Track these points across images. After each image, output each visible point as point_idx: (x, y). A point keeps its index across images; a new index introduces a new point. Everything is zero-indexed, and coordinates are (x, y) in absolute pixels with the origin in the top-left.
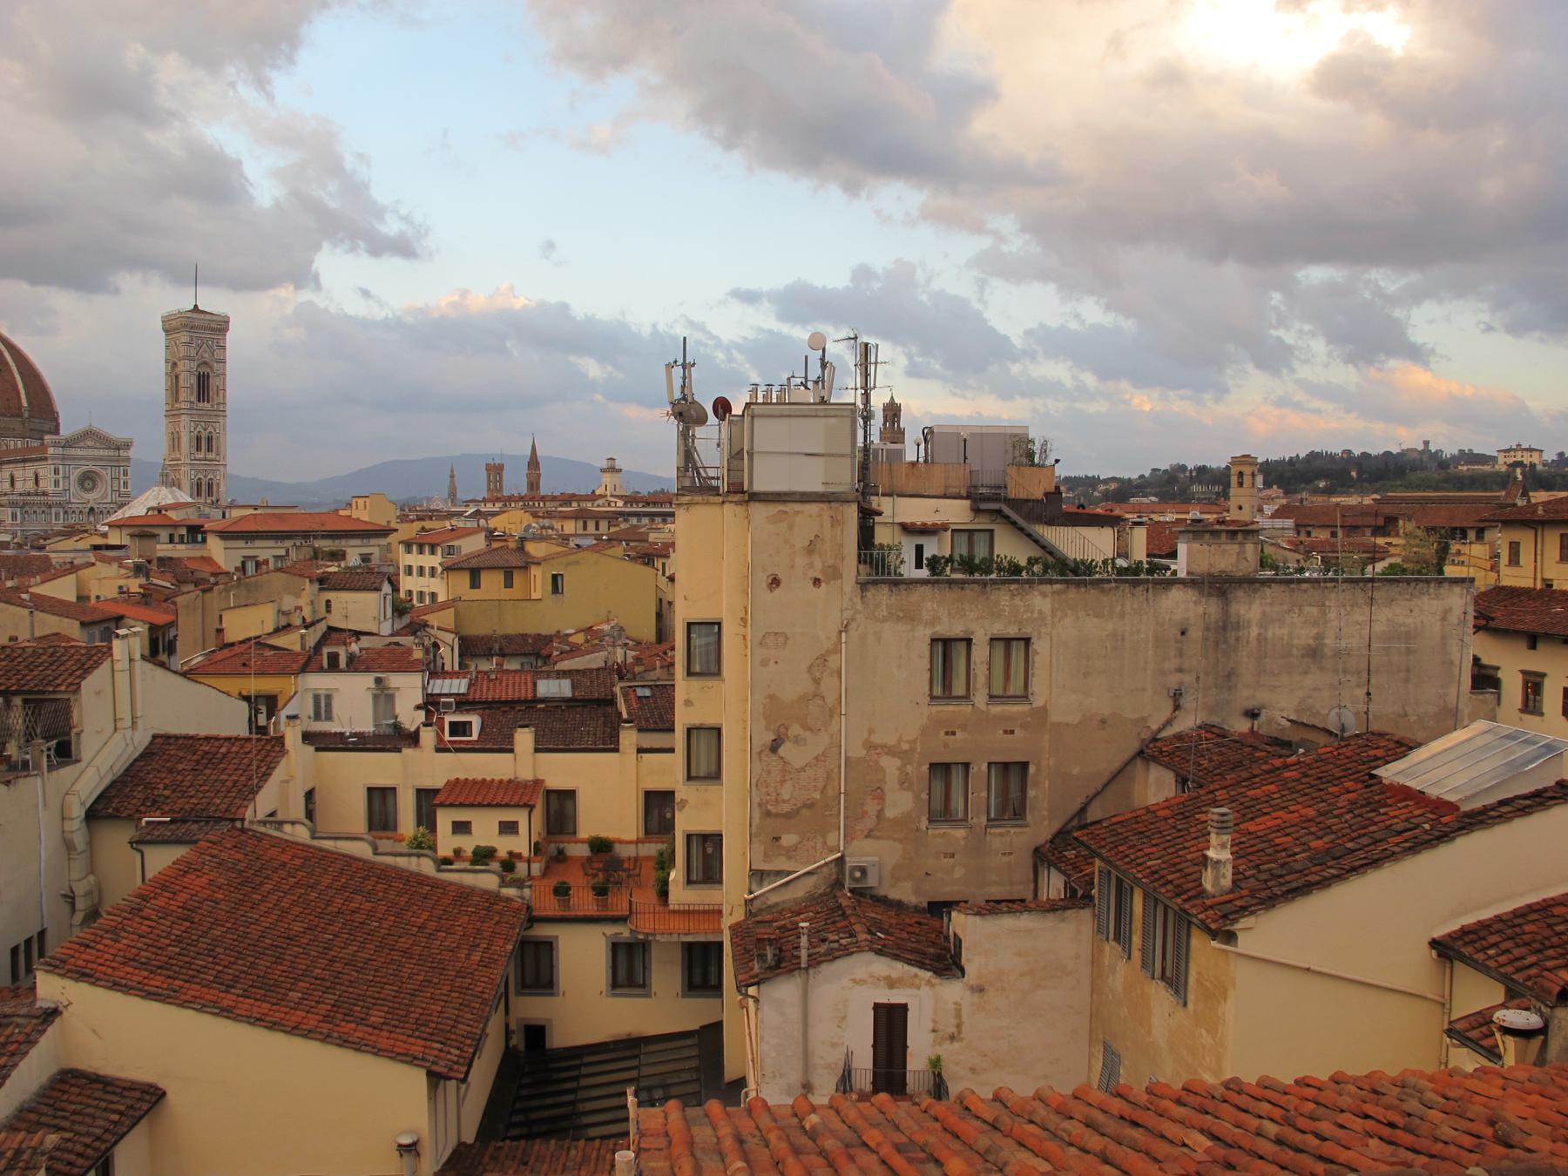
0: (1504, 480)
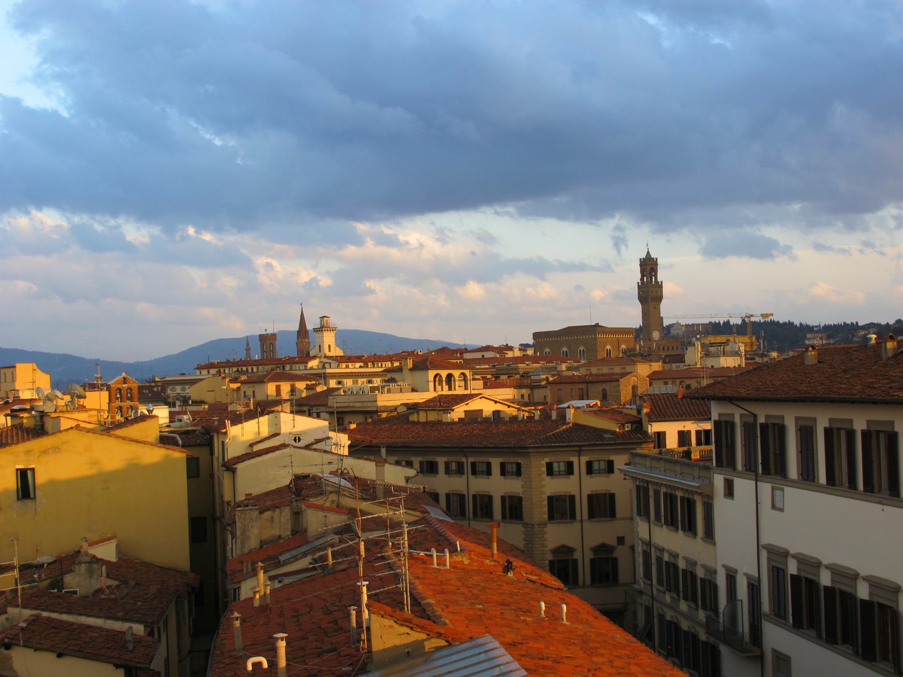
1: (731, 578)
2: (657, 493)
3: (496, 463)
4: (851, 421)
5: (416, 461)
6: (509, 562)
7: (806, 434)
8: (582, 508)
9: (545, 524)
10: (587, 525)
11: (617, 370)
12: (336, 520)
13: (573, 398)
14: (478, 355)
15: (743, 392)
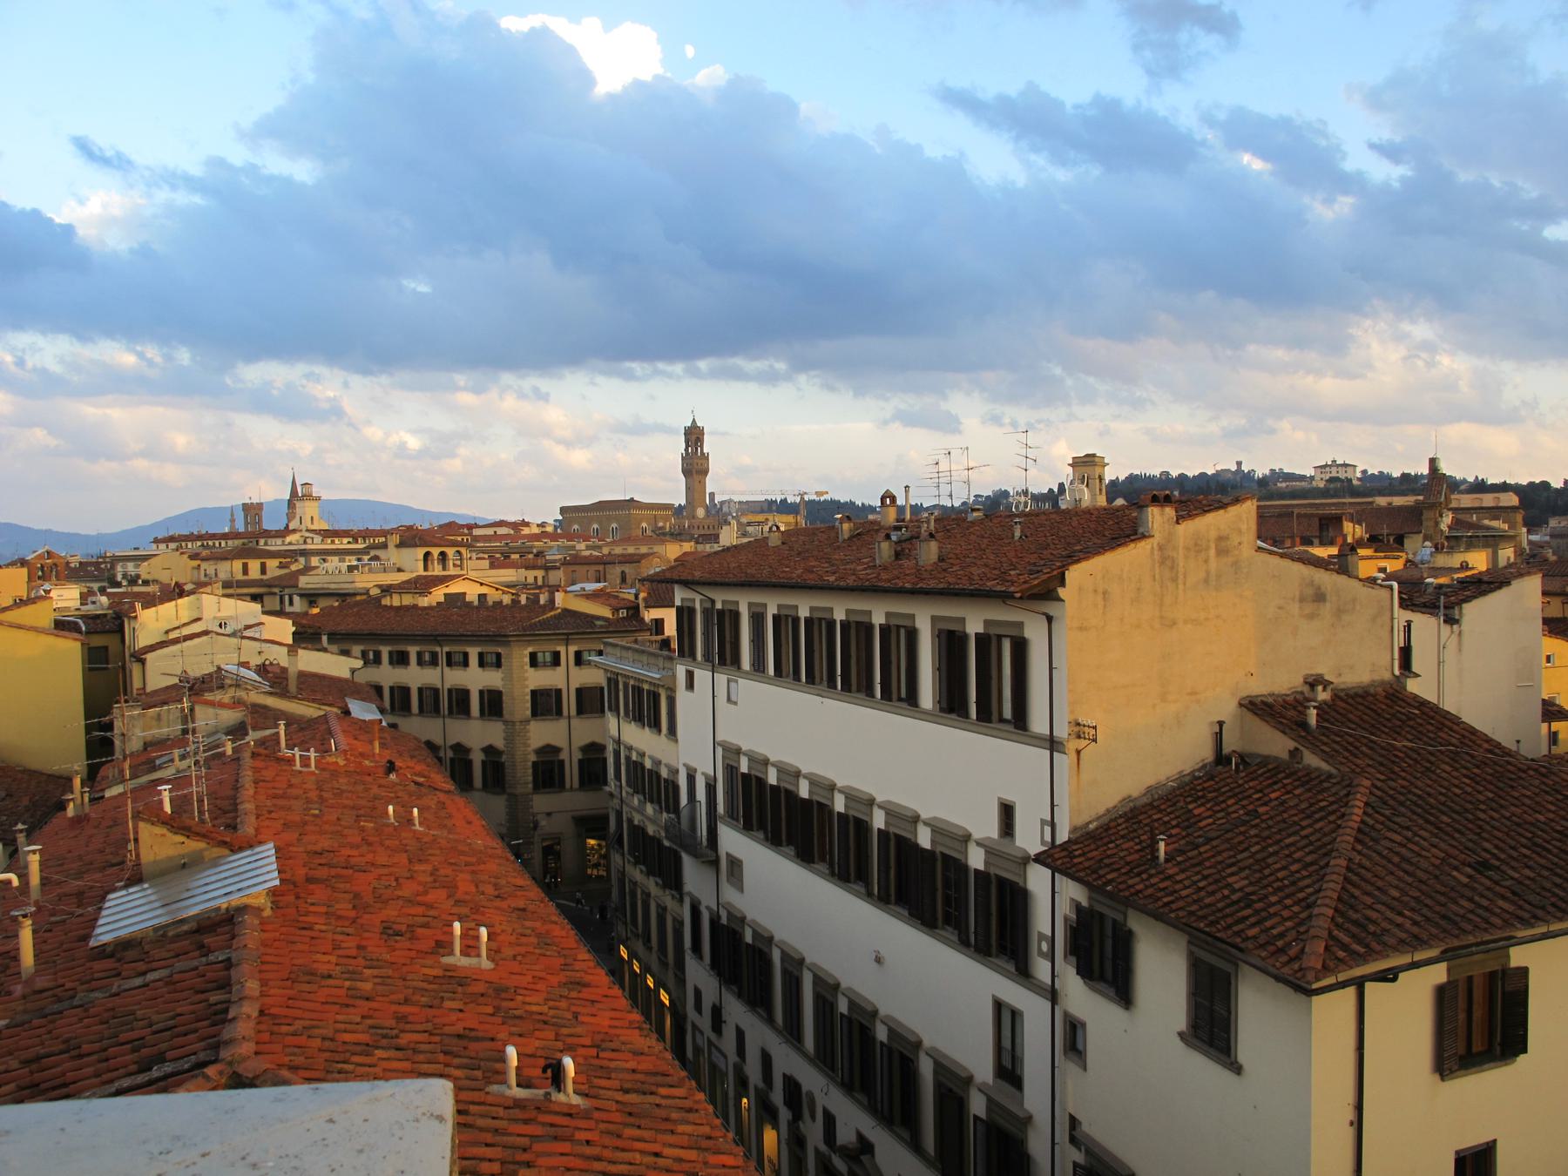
0: (1324, 493)
1: (691, 779)
2: (626, 685)
3: (474, 653)
5: (357, 649)
6: (391, 763)
7: (758, 619)
8: (570, 703)
9: (528, 721)
10: (573, 722)
11: (644, 550)
12: (230, 717)
13: (588, 580)
14: (490, 531)
15: (698, 575)
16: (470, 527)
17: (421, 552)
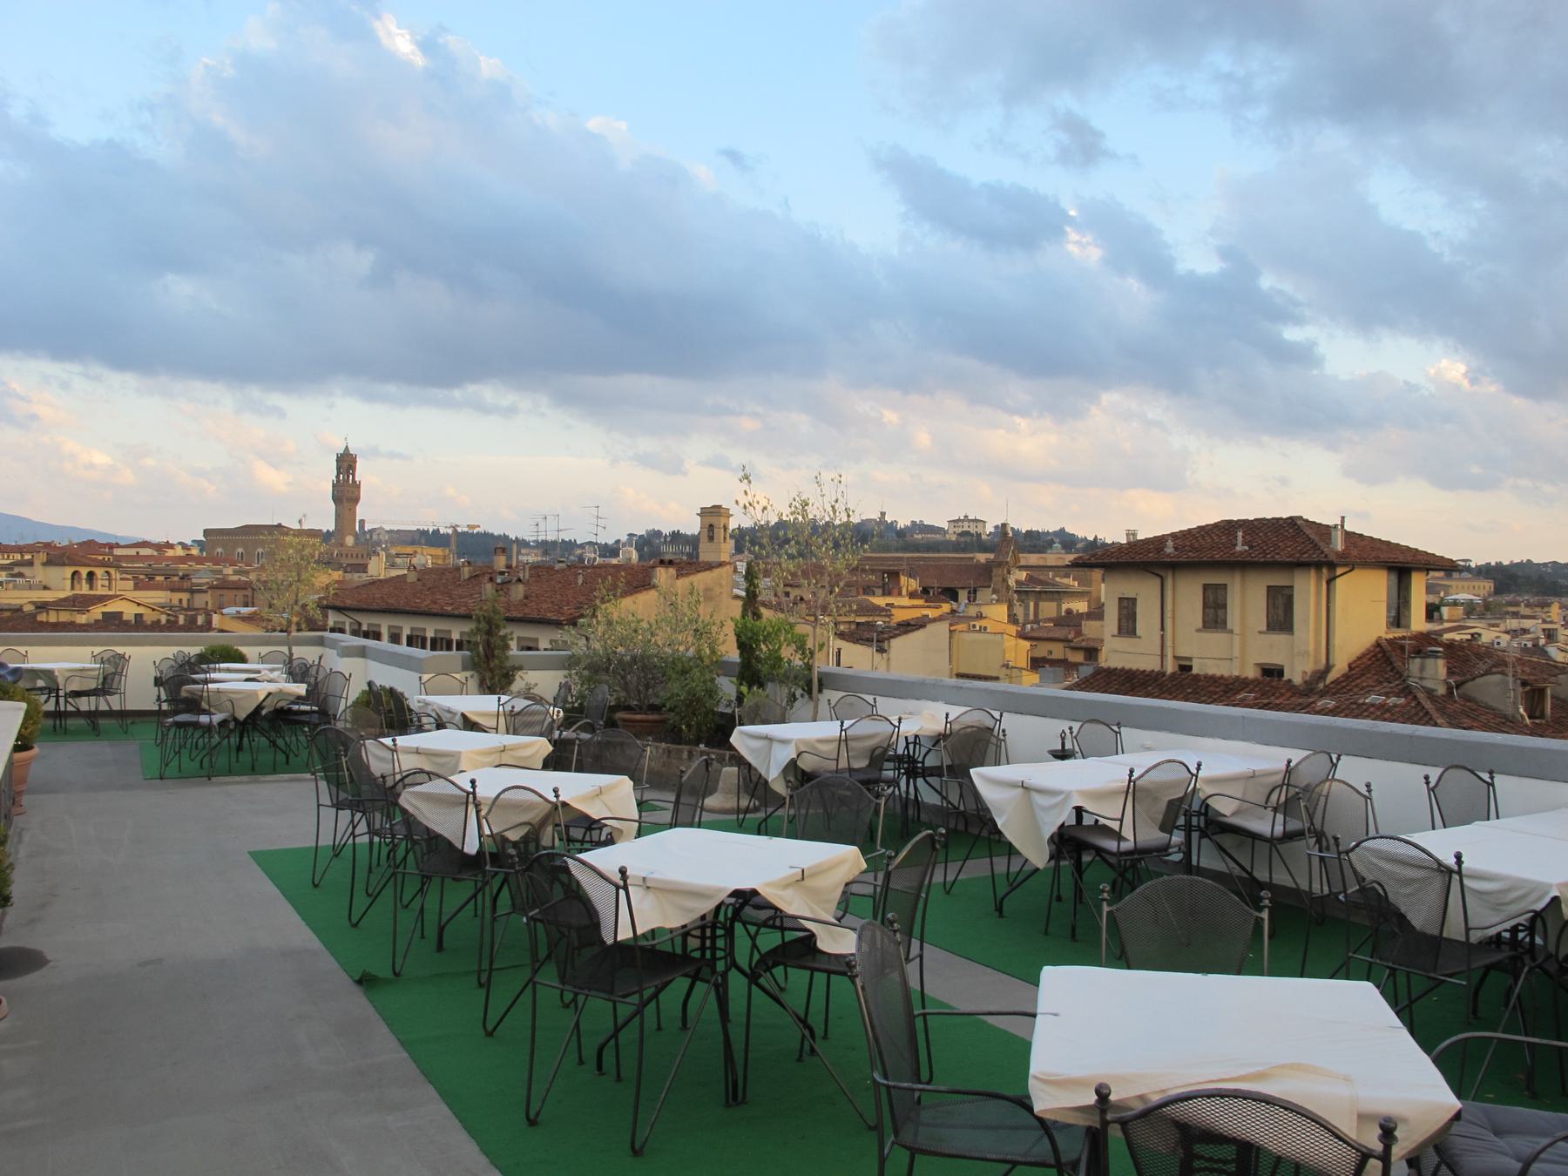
0: (956, 547)
4: (449, 632)
14: (132, 552)
15: (349, 602)
16: (111, 546)
17: (69, 571)
